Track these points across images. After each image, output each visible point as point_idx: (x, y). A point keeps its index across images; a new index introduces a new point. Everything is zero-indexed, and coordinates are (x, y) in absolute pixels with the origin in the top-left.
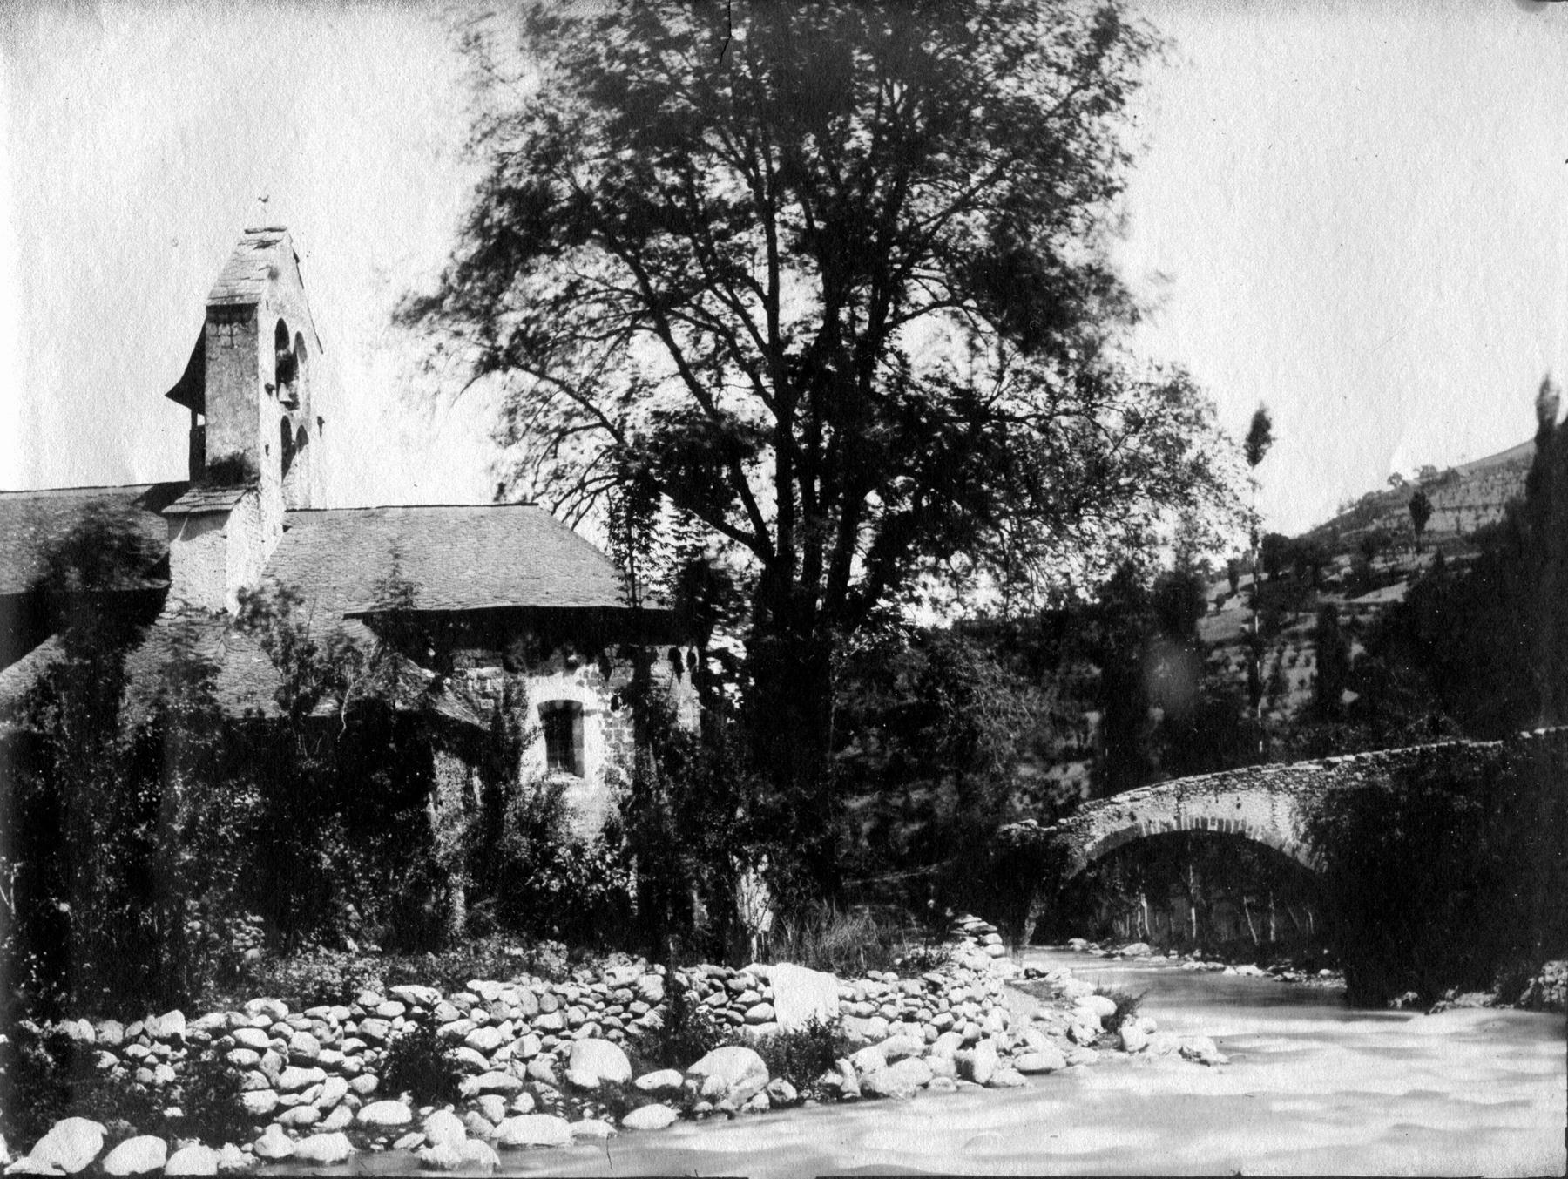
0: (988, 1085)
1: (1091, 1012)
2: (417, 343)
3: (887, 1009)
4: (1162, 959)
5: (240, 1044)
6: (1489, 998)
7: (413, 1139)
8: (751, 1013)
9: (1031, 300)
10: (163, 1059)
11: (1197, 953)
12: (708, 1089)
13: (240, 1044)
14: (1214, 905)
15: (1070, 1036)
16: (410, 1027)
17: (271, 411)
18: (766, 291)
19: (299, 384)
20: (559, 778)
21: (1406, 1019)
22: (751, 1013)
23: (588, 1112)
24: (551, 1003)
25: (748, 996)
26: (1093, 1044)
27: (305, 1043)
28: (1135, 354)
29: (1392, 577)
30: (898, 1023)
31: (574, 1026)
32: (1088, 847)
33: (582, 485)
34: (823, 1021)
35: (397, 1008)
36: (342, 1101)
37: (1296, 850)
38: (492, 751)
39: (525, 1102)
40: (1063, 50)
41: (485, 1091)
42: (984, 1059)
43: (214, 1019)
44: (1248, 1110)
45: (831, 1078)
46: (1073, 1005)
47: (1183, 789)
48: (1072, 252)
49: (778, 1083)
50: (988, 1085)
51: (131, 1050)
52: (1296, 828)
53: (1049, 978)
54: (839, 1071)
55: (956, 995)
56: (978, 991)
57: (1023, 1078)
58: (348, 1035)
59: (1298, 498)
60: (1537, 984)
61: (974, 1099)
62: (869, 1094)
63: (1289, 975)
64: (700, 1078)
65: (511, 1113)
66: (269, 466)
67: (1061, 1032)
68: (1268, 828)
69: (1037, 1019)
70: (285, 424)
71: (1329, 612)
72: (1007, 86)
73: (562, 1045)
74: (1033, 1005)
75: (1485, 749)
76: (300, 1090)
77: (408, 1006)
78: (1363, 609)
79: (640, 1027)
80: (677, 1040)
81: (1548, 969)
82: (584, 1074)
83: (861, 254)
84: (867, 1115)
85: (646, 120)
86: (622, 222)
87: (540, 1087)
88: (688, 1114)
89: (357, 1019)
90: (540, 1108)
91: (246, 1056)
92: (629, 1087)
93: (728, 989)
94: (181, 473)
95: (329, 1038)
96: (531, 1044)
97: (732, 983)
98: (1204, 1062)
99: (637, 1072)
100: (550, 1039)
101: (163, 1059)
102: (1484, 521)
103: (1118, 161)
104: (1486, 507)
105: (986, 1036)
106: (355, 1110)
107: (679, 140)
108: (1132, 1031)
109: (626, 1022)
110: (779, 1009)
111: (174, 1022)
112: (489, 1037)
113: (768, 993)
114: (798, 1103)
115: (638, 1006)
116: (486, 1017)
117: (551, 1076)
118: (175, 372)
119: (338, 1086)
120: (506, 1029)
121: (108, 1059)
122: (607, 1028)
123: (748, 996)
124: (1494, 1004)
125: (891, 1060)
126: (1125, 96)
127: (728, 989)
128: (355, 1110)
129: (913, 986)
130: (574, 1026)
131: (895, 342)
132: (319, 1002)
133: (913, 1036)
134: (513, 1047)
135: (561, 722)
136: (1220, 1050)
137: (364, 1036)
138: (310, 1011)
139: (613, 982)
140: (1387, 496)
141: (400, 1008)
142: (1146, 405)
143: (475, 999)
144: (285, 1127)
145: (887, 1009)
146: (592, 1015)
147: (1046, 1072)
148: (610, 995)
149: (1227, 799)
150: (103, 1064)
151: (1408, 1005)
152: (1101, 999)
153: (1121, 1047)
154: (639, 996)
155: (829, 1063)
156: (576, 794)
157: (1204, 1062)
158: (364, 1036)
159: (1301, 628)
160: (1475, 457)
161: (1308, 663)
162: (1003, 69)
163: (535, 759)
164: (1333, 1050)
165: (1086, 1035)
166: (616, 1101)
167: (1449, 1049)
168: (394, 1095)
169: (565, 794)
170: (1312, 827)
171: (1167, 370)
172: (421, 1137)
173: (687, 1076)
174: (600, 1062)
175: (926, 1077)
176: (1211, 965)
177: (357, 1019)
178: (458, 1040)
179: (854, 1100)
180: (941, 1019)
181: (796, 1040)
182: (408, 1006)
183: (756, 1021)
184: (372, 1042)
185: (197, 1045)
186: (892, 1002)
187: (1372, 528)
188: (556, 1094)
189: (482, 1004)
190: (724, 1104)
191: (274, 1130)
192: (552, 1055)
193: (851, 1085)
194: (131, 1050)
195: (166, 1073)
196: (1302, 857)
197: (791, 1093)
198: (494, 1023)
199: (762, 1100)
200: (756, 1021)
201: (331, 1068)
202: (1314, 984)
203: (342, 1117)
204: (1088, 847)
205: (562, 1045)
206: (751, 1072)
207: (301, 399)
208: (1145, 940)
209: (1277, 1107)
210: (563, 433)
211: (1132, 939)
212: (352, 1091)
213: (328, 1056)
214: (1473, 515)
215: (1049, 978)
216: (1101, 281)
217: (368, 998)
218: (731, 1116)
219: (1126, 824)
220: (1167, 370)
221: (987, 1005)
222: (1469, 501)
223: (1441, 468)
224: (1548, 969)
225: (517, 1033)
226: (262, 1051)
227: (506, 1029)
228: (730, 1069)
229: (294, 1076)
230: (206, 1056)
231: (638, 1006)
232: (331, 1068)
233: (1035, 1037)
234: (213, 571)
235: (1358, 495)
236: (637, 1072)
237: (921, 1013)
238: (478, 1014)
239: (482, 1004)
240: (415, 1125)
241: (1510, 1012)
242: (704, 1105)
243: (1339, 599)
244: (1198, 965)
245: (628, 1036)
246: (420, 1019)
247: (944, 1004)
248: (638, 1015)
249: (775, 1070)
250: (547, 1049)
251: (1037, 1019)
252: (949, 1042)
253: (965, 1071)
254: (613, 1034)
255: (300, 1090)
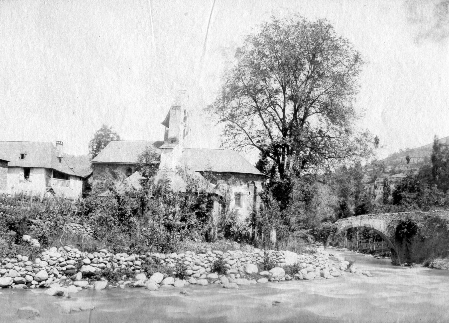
0: (327, 278)
1: (344, 264)
2: (207, 114)
3: (306, 261)
4: (350, 252)
5: (186, 260)
6: (422, 265)
7: (218, 282)
8: (281, 260)
9: (332, 112)
10: (172, 262)
11: (358, 251)
12: (273, 276)
13: (186, 260)
14: (367, 242)
15: (340, 269)
16: (217, 259)
17: (182, 128)
18: (283, 108)
19: (187, 122)
20: (238, 208)
21: (405, 269)
22: (281, 260)
23: (250, 279)
24: (243, 256)
25: (280, 257)
26: (345, 271)
27: (198, 261)
28: (358, 126)
29: (400, 172)
30: (308, 264)
31: (247, 261)
32: (341, 228)
33: (240, 145)
34: (296, 263)
35: (215, 255)
36: (204, 273)
37: (384, 232)
38: (224, 203)
39: (238, 276)
40: (348, 63)
41: (231, 273)
42: (326, 272)
43: (182, 255)
44: (384, 287)
45: (297, 275)
46: (340, 262)
47: (362, 218)
48: (346, 104)
49: (287, 275)
50: (327, 278)
51: (167, 260)
52: (384, 227)
53: (334, 256)
54: (299, 274)
55: (320, 259)
56: (324, 259)
57: (333, 277)
58: (205, 260)
59: (382, 155)
60: (433, 264)
61: (324, 280)
62: (304, 279)
63: (379, 258)
64: (272, 273)
65: (236, 278)
66: (180, 139)
67: (338, 268)
68: (379, 227)
69: (333, 265)
70: (184, 130)
71: (386, 179)
72: (335, 69)
73: (244, 265)
74: (333, 262)
75: (425, 214)
76: (197, 270)
77: (217, 255)
78: (393, 178)
79: (260, 262)
80: (267, 266)
81: (435, 260)
82: (249, 271)
83: (301, 102)
84: (304, 282)
85: (259, 72)
86: (252, 92)
87: (241, 273)
88: (270, 280)
89: (207, 257)
90: (241, 277)
91: (188, 263)
92: (258, 274)
93: (276, 255)
94: (162, 139)
95: (202, 260)
96: (239, 264)
97: (277, 254)
98: (368, 276)
99: (259, 271)
100: (243, 263)
101: (172, 262)
102: (419, 161)
103: (358, 87)
104: (420, 158)
105: (325, 268)
106: (207, 275)
107: (264, 75)
108: (353, 268)
109: (257, 261)
110: (286, 260)
111: (174, 255)
112: (231, 262)
113: (284, 256)
114: (291, 280)
115: (259, 258)
116: (231, 258)
117: (243, 271)
118: (163, 119)
119: (203, 270)
120: (235, 260)
121: (162, 261)
122: (253, 262)
123: (280, 257)
124: (423, 267)
125: (308, 272)
126: (359, 73)
127: (276, 255)
128: (207, 275)
129: (311, 257)
130: (247, 261)
131: (308, 120)
132: (200, 253)
133: (311, 267)
134: (236, 264)
135: (238, 195)
136: (371, 274)
137: (208, 260)
138: (199, 255)
139: (255, 253)
140: (398, 154)
141: (215, 255)
142: (359, 137)
143: (229, 254)
144: (194, 277)
145: (306, 261)
146: (251, 259)
147: (338, 276)
148: (254, 255)
149: (371, 221)
150: (161, 262)
151: (406, 266)
152: (346, 261)
153: (351, 272)
154: (259, 256)
155: (297, 272)
156: (240, 212)
157: (368, 276)
158: (208, 260)
159: (380, 181)
160: (418, 146)
161: (381, 189)
162: (334, 65)
163: (232, 205)
164: (393, 275)
165: (343, 269)
166: (256, 276)
167: (415, 276)
168: (214, 272)
169: (238, 211)
170: (388, 227)
171: (365, 130)
172: (220, 281)
173: (270, 273)
174: (252, 269)
175: (315, 276)
176: (361, 254)
177: (207, 257)
178: (226, 262)
179: (302, 280)
180: (317, 264)
181: (291, 267)
182: (217, 255)
183: (281, 262)
184: (210, 262)
185: (178, 260)
186: (307, 260)
187: (395, 160)
188: (244, 274)
189: (231, 255)
190: (277, 279)
191: (192, 278)
192: (243, 266)
193: (301, 277)
194: (167, 260)
195: (173, 265)
196: (385, 234)
197: (290, 278)
198: (232, 259)
199: (284, 279)
200: (281, 262)
201: (202, 266)
202: (384, 260)
203: (204, 276)
204: (341, 228)
205: (244, 265)
206: (282, 273)
207: (187, 125)
208: (346, 247)
209: (389, 287)
210: (236, 134)
211: (343, 247)
212: (206, 271)
213: (202, 264)
214: (417, 159)
215: (334, 256)
216: (351, 110)
217: (209, 252)
218: (278, 281)
219: (350, 224)
220: (365, 130)
221: (326, 262)
222: (416, 156)
223: (411, 148)
224: (435, 260)
225: (237, 262)
226: (190, 262)
227: (235, 260)
228: (277, 272)
229: (196, 267)
230: (180, 262)
231: (259, 258)
232: (202, 266)
233: (334, 269)
234: (169, 161)
235: (392, 153)
236: (259, 271)
237: (313, 263)
238: (230, 257)
239: (231, 255)
240: (219, 279)
241: (427, 269)
242: (273, 279)
243: (388, 176)
244: (358, 254)
245: (257, 263)
246: (219, 258)
247: (317, 261)
248: (259, 260)
249: (287, 273)
250: (242, 265)
251: (333, 265)
252: (318, 269)
253: (322, 275)
254: (254, 263)
255: (197, 270)
